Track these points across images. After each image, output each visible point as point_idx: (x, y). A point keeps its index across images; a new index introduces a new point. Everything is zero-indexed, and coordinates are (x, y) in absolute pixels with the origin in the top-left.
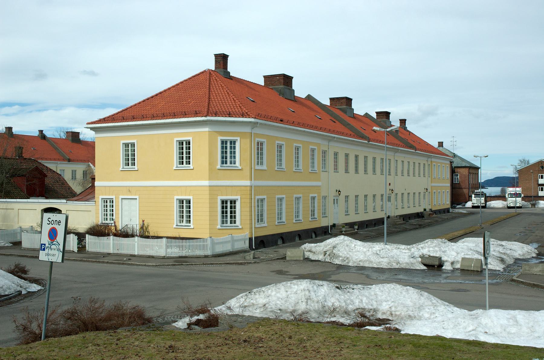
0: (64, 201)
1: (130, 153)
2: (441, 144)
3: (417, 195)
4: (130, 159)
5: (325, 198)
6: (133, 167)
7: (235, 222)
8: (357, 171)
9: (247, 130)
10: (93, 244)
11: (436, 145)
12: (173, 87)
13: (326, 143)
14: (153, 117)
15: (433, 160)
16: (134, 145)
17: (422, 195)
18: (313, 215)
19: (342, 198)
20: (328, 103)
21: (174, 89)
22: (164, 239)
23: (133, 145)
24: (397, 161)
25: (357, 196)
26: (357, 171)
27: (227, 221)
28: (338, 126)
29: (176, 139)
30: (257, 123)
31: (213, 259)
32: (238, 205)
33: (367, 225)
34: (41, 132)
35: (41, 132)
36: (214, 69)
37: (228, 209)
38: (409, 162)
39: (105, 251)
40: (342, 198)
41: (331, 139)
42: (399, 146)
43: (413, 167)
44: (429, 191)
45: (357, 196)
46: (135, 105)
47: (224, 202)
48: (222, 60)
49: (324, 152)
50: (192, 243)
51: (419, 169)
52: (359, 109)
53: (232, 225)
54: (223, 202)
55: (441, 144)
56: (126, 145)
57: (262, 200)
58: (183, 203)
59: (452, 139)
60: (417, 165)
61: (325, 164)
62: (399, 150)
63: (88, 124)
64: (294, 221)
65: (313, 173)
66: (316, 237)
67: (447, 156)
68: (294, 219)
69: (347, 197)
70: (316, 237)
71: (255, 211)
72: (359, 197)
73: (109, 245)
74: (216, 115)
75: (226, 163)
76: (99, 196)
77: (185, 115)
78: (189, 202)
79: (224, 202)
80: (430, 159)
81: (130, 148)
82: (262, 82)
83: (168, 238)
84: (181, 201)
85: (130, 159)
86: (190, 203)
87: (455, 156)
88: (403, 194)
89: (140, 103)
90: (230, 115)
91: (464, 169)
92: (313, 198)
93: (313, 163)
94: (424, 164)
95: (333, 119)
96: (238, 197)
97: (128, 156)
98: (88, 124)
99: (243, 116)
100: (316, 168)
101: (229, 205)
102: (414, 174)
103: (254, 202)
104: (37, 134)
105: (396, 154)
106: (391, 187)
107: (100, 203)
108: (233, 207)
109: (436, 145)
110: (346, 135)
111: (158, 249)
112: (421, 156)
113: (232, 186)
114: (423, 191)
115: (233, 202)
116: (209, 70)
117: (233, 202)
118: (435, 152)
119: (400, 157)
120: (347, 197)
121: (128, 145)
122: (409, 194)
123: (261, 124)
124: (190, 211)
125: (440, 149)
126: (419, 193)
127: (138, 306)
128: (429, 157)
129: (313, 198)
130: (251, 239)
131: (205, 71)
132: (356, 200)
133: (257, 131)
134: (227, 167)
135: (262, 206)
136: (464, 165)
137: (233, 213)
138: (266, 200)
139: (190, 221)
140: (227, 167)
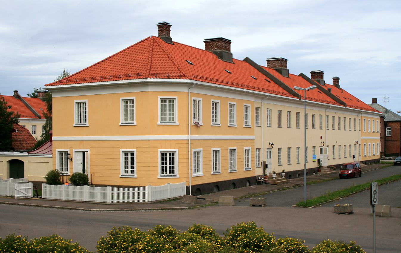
0: (26, 154)
1: (82, 111)
2: (375, 101)
3: (348, 147)
4: (82, 117)
5: (258, 150)
6: (85, 123)
7: (173, 172)
8: (289, 126)
9: (185, 90)
10: (49, 192)
11: (369, 102)
12: (121, 52)
13: (259, 101)
14: (102, 79)
15: (363, 115)
16: (86, 104)
17: (353, 147)
18: (232, 166)
19: (275, 151)
20: (264, 64)
21: (122, 53)
22: (108, 187)
23: (85, 104)
24: (328, 116)
25: (289, 149)
26: (289, 126)
27: (166, 171)
28: (273, 86)
29: (121, 99)
30: (193, 84)
31: (151, 205)
32: (176, 157)
33: (299, 174)
34: (16, 92)
35: (16, 92)
36: (157, 36)
37: (168, 161)
38: (339, 117)
39: (60, 198)
40: (275, 151)
41: (263, 97)
42: (330, 103)
43: (332, 123)
44: (359, 143)
45: (289, 149)
46: (88, 68)
47: (163, 154)
48: (164, 28)
49: (258, 109)
50: (133, 191)
51: (350, 124)
52: (294, 68)
53: (170, 175)
54: (162, 154)
55: (375, 101)
56: (78, 104)
57: (198, 152)
58: (127, 155)
59: (385, 96)
60: (347, 120)
61: (258, 120)
62: (329, 106)
63: (45, 86)
64: (244, 170)
65: (248, 127)
66: (250, 185)
67: (378, 111)
68: (244, 168)
69: (280, 149)
70: (250, 185)
71: (191, 162)
72: (282, 150)
73: (65, 192)
74: (156, 77)
75: (166, 120)
76: (57, 149)
77: (129, 77)
78: (133, 154)
79: (163, 154)
80: (360, 115)
81: (82, 107)
82: (203, 47)
83: (112, 186)
84: (126, 154)
85: (82, 117)
86: (133, 155)
87: (387, 111)
88: (334, 146)
89: (91, 67)
90: (168, 77)
91: (396, 124)
92: (247, 150)
93: (247, 119)
94: (355, 119)
95: (268, 79)
96: (176, 150)
97: (81, 114)
98: (45, 86)
99: (180, 77)
100: (250, 124)
101: (168, 157)
102: (345, 128)
103: (191, 155)
104: (12, 94)
105: (327, 110)
106: (323, 140)
107: (58, 156)
108: (172, 159)
109: (369, 102)
110: (279, 93)
111: (107, 196)
112: (353, 112)
113: (171, 140)
114: (353, 143)
115: (172, 154)
116: (152, 36)
117: (172, 154)
118: (372, 108)
119: (331, 113)
120: (280, 149)
121: (81, 104)
122: (340, 146)
123: (196, 84)
124: (133, 162)
125: (375, 106)
126: (350, 145)
127: (252, 228)
128: (359, 112)
129: (247, 150)
130: (188, 188)
131: (149, 38)
132: (289, 152)
133: (193, 91)
134: (166, 123)
135: (198, 158)
136: (396, 120)
137: (172, 163)
138: (202, 151)
139: (134, 171)
140: (166, 123)
